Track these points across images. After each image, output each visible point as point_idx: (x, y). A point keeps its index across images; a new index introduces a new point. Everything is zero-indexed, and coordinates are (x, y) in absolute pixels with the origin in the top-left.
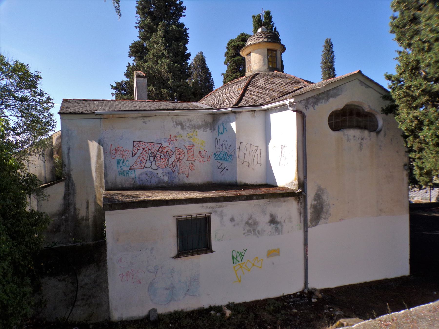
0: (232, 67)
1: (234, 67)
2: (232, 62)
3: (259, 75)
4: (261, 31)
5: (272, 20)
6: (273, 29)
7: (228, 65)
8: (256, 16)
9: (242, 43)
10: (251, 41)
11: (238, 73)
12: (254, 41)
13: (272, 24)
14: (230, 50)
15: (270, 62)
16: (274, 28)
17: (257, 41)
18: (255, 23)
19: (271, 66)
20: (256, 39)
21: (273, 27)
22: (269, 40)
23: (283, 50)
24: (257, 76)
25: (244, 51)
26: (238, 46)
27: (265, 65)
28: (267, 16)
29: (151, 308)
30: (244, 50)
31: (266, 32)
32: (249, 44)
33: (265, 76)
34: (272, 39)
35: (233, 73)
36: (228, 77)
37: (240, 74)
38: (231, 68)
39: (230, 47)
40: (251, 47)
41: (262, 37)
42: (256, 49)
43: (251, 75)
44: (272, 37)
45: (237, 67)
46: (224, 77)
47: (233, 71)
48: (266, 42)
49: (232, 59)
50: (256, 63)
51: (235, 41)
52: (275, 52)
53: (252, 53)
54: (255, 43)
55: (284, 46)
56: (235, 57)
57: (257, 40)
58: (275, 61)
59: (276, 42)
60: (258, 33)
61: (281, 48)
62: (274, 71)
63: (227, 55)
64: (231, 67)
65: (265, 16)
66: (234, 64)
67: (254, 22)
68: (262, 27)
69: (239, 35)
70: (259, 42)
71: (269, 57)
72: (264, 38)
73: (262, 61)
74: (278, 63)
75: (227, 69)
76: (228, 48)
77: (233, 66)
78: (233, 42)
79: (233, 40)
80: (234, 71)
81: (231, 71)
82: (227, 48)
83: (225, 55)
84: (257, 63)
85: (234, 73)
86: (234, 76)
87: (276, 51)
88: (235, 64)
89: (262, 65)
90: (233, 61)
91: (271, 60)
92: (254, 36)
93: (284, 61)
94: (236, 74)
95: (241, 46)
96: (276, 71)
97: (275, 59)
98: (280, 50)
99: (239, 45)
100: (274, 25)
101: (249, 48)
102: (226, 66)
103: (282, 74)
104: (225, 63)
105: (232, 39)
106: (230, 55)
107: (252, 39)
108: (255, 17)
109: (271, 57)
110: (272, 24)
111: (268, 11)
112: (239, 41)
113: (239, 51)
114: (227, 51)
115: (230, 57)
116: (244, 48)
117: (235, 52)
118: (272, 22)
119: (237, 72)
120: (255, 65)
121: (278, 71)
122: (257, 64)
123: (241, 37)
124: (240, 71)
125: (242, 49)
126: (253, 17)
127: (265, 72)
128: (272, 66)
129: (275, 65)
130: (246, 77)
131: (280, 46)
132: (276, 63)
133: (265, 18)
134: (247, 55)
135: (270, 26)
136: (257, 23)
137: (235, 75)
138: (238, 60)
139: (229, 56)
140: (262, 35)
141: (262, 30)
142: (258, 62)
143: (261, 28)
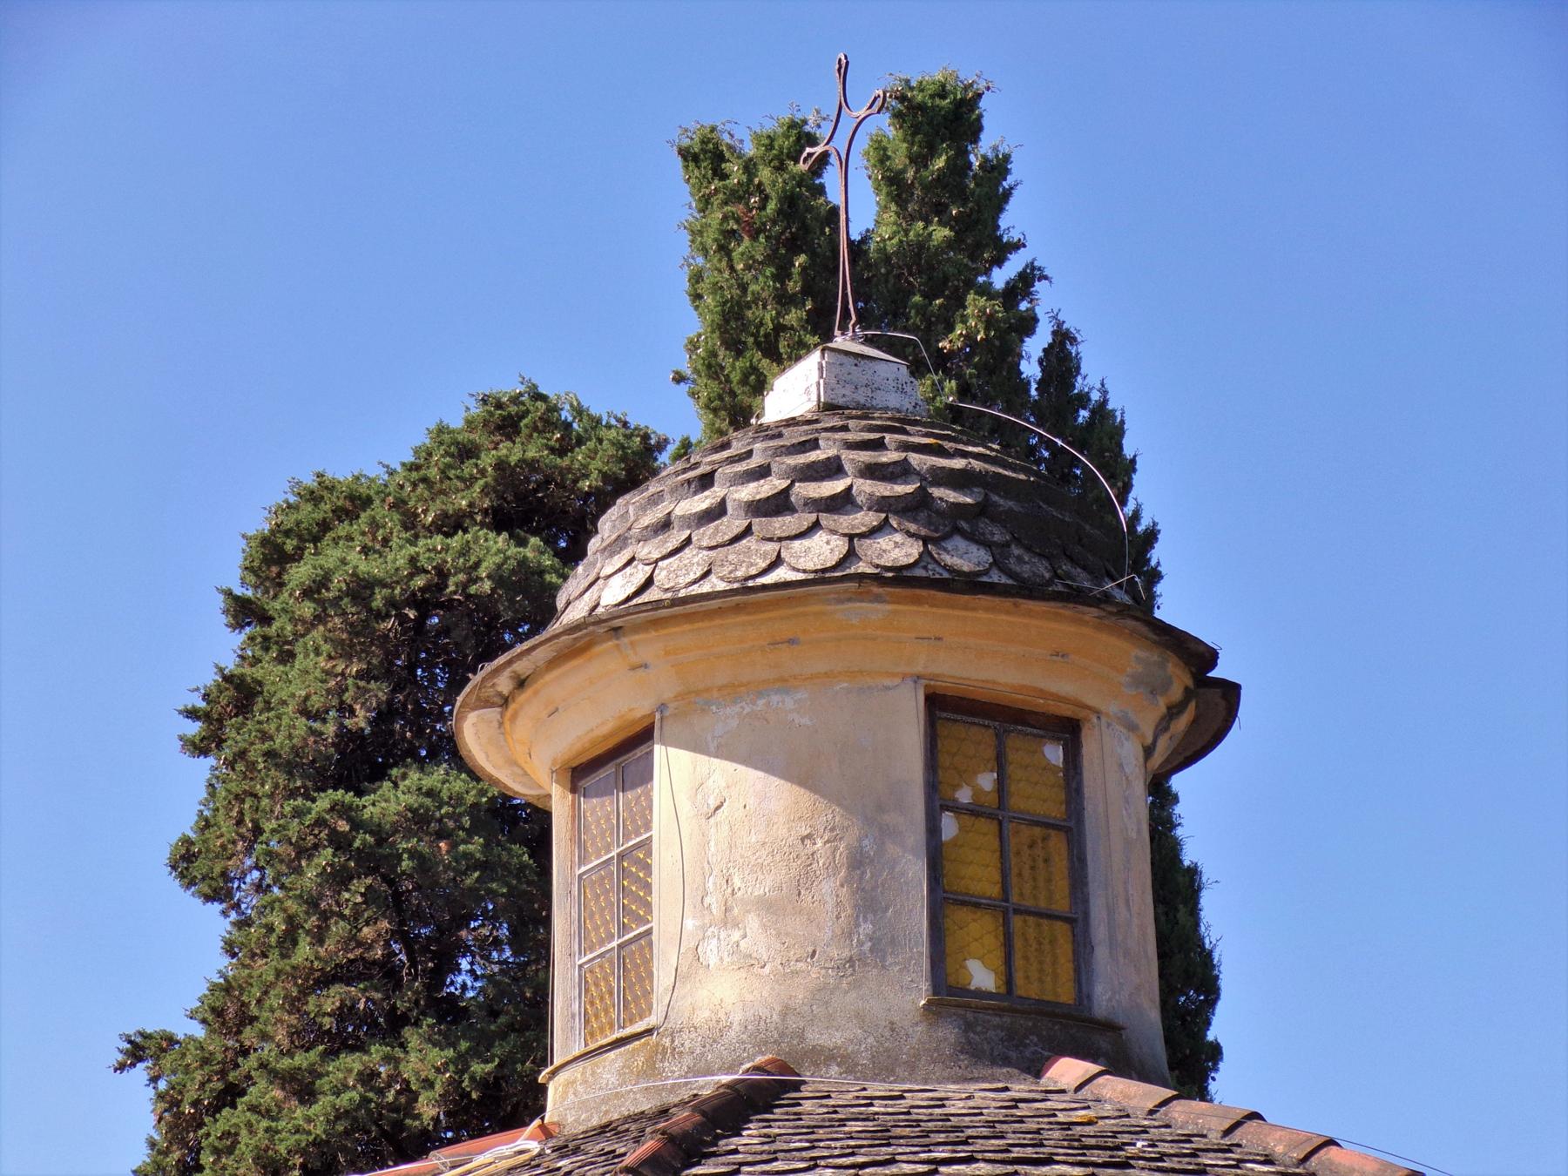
0: (319, 938)
1: (353, 940)
2: (326, 856)
3: (779, 1122)
4: (828, 407)
5: (1011, 222)
6: (1031, 369)
7: (250, 902)
8: (750, 150)
9: (494, 549)
10: (650, 550)
11: (412, 1036)
12: (694, 560)
13: (1000, 277)
14: (286, 657)
15: (973, 903)
16: (1035, 346)
17: (752, 557)
18: (724, 250)
19: (982, 977)
20: (733, 523)
21: (1028, 325)
22: (963, 557)
23: (1182, 723)
24: (750, 1136)
25: (529, 706)
26: (425, 602)
27: (880, 949)
28: (919, 161)
29: (173, 884)
30: (521, 683)
31: (901, 424)
32: (614, 592)
33: (884, 1136)
34: (998, 535)
35: (323, 1034)
36: (230, 1095)
37: (461, 1063)
38: (304, 950)
39: (288, 606)
40: (648, 647)
41: (842, 503)
42: (733, 691)
43: (647, 1105)
44: (1002, 502)
45: (400, 934)
46: (169, 1101)
47: (332, 998)
48: (900, 578)
49: (323, 802)
50: (728, 920)
51: (379, 510)
52: (1054, 754)
53: (658, 750)
54: (715, 584)
55: (1199, 657)
56: (379, 774)
57: (754, 554)
58: (1062, 904)
59: (1075, 596)
60: (772, 433)
61: (1166, 686)
62: (1036, 1069)
63: (235, 738)
64: (289, 940)
65: (899, 160)
66: (353, 895)
67: (710, 238)
68: (840, 341)
69: (456, 422)
70: (781, 574)
71: (949, 826)
72: (864, 519)
73: (829, 891)
74: (1099, 932)
75: (215, 964)
76: (266, 620)
77: (338, 928)
78: (342, 529)
79: (355, 503)
80: (345, 1012)
81: (294, 1004)
82: (243, 612)
83: (194, 728)
84: (753, 923)
85: (339, 1043)
86: (344, 1100)
87: (1068, 730)
88: (370, 896)
89: (838, 953)
90: (340, 843)
91: (980, 876)
92: (706, 481)
93: (1207, 874)
94: (377, 1051)
95: (484, 604)
96: (1067, 1071)
97: (1065, 948)
98: (1132, 728)
99: (442, 573)
100: (1046, 301)
101: (606, 661)
102: (213, 922)
103: (1185, 1113)
104: (185, 861)
105: (341, 472)
106: (290, 731)
107: (665, 525)
108: (734, 168)
109: (987, 827)
110: (1000, 277)
111: (942, 92)
112: (451, 524)
113: (457, 684)
114: (230, 663)
115: (290, 768)
116: (525, 656)
117: (380, 691)
118: (1004, 250)
119: (392, 1027)
120: (711, 952)
121: (1121, 1063)
122: (754, 935)
123: (487, 460)
124: (450, 1012)
125: (494, 676)
126: (687, 155)
127: (884, 1067)
128: (1009, 981)
129: (1066, 968)
130: (546, 1132)
131: (1133, 655)
132: (1077, 922)
133: (895, 187)
134: (580, 774)
135: (974, 304)
136: (760, 249)
137: (368, 1077)
138: (418, 820)
139: (270, 755)
140: (832, 469)
141: (843, 395)
142: (767, 906)
143: (812, 362)
